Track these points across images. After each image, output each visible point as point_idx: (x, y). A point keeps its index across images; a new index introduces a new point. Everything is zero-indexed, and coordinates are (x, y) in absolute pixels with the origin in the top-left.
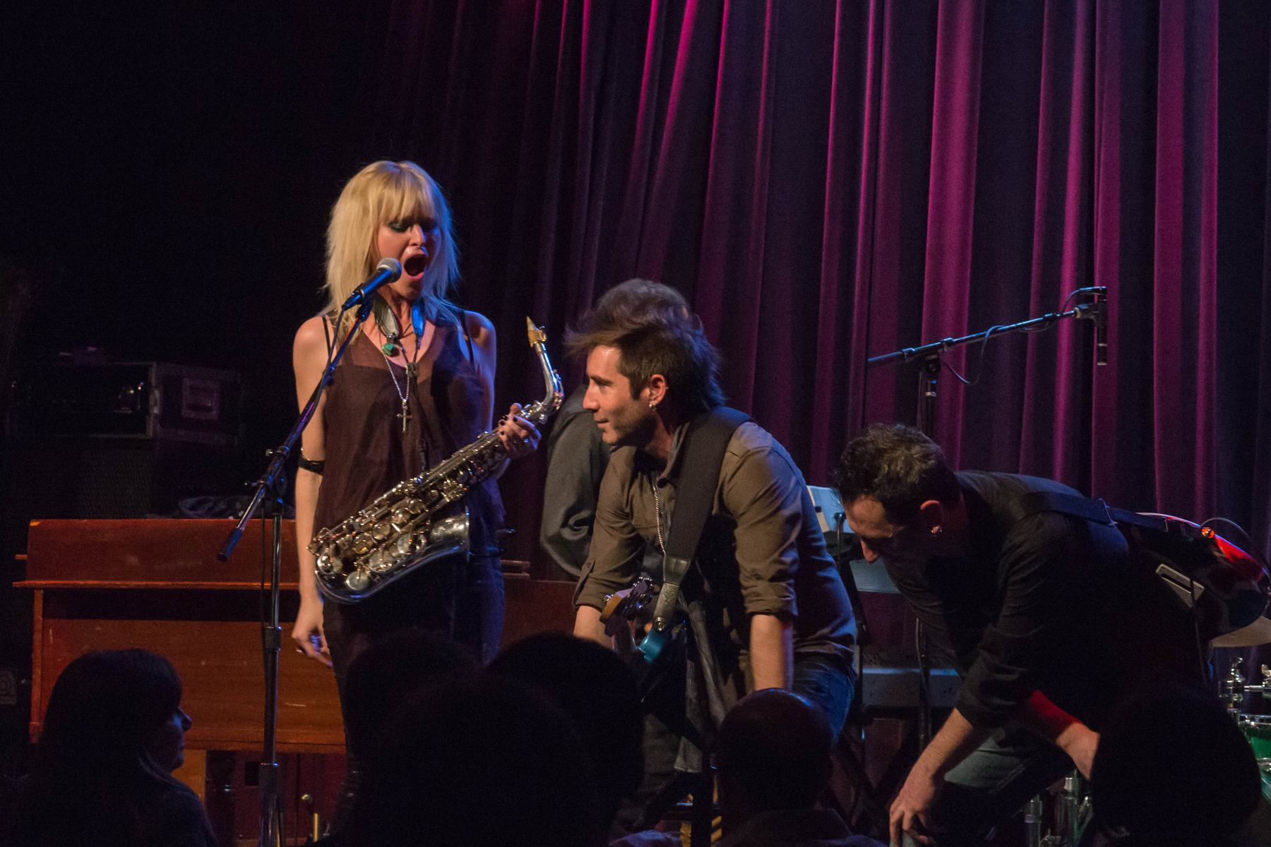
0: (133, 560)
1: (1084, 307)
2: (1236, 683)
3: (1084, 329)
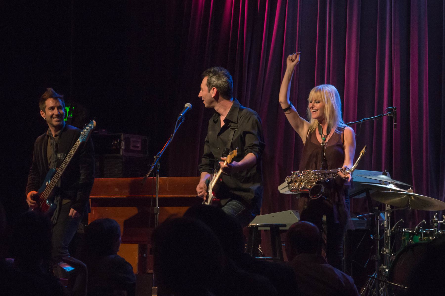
0: (117, 190)
1: (390, 113)
2: (435, 221)
3: (391, 120)
